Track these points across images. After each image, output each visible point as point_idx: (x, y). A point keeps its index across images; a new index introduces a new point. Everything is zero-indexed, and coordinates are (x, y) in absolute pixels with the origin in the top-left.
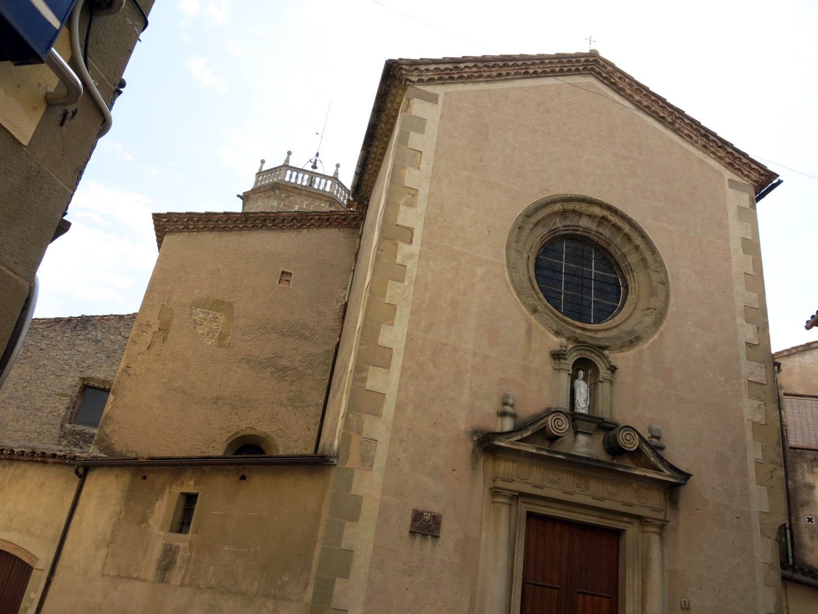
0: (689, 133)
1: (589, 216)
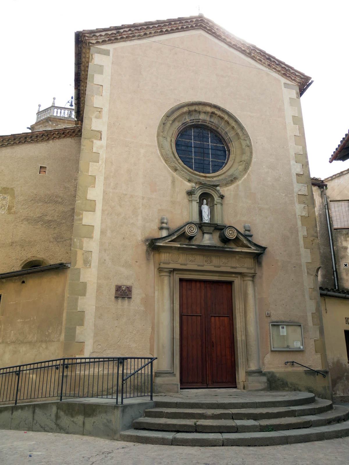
0: (260, 58)
1: (205, 113)
